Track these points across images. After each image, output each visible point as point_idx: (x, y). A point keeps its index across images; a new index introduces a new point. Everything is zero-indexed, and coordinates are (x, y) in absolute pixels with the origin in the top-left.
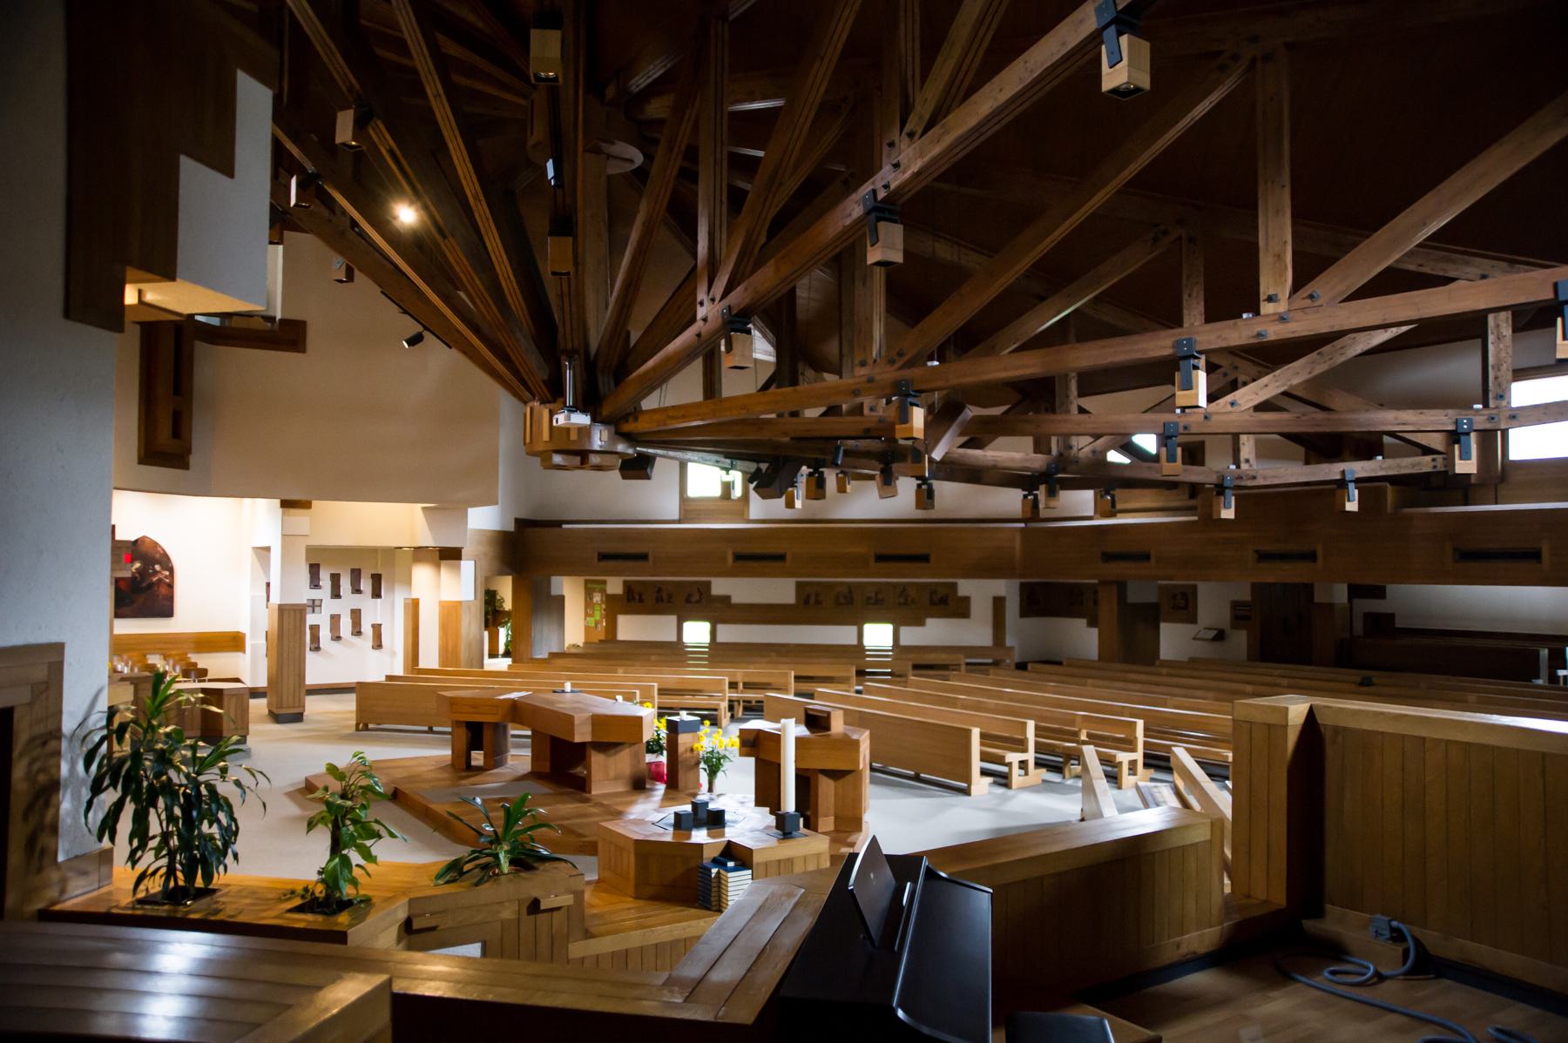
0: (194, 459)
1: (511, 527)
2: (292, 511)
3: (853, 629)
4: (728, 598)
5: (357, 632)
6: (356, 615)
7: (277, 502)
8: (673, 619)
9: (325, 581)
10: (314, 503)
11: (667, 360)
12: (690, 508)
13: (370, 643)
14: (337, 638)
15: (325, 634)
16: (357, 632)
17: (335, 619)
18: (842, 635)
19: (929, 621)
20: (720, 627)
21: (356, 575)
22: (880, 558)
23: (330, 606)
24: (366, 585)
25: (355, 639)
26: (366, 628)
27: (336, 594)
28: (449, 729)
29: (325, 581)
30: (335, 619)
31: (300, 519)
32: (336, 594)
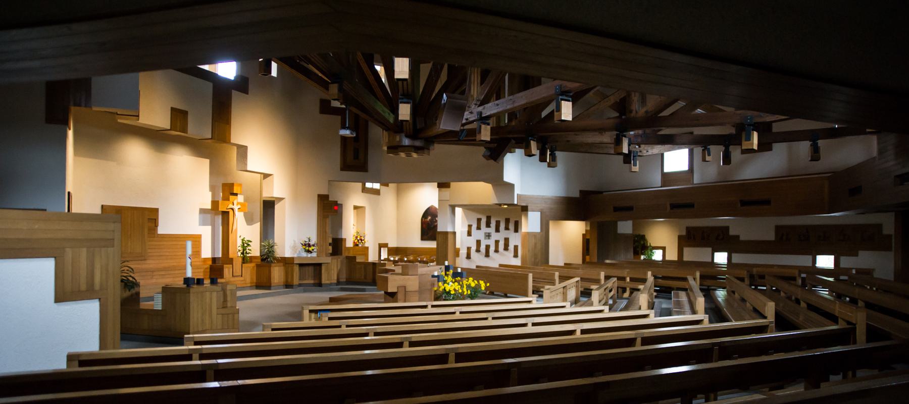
0: (371, 165)
1: (577, 195)
2: (443, 189)
3: (810, 257)
4: (738, 237)
5: (506, 248)
6: (507, 240)
7: (436, 184)
8: (710, 249)
9: (493, 224)
10: (452, 184)
11: (307, 69)
12: (668, 178)
13: (512, 254)
14: (496, 251)
15: (492, 249)
16: (506, 248)
17: (497, 242)
18: (802, 260)
19: (861, 253)
20: (734, 255)
21: (507, 221)
22: (744, 203)
23: (495, 236)
24: (512, 226)
25: (506, 252)
26: (511, 247)
27: (497, 230)
28: (312, 282)
29: (493, 224)
30: (497, 242)
31: (446, 191)
32: (497, 230)
